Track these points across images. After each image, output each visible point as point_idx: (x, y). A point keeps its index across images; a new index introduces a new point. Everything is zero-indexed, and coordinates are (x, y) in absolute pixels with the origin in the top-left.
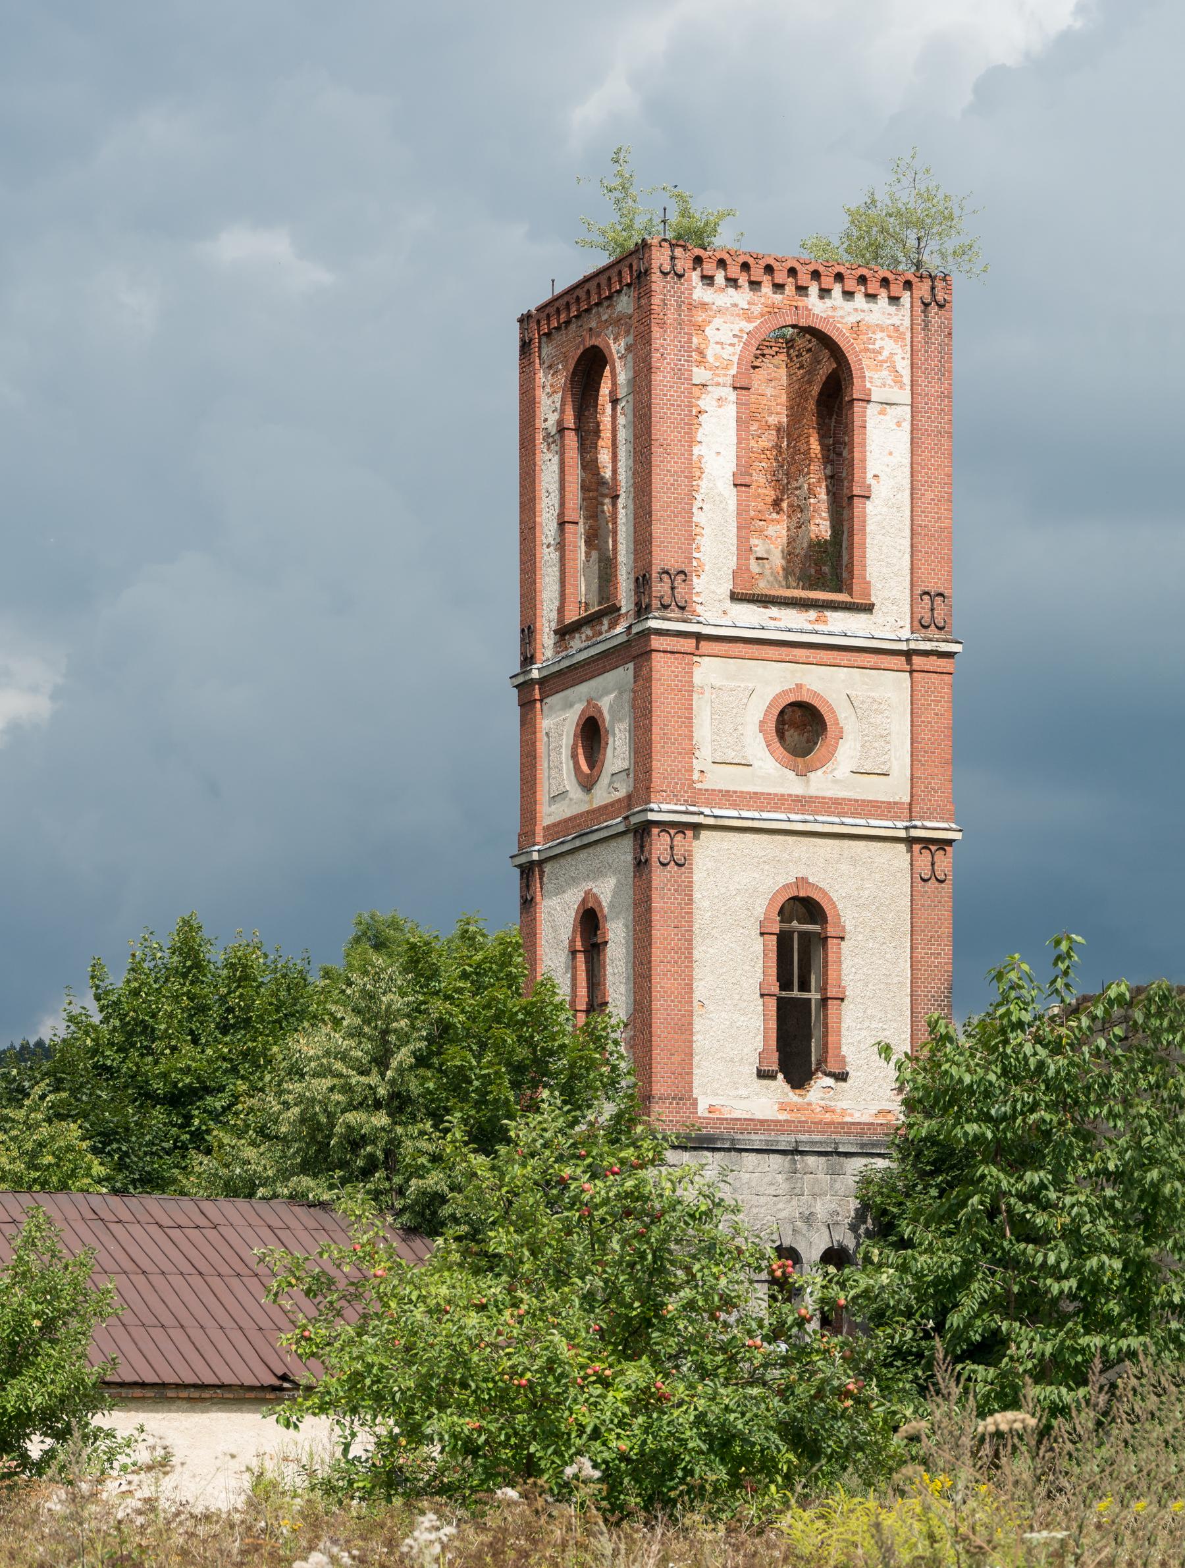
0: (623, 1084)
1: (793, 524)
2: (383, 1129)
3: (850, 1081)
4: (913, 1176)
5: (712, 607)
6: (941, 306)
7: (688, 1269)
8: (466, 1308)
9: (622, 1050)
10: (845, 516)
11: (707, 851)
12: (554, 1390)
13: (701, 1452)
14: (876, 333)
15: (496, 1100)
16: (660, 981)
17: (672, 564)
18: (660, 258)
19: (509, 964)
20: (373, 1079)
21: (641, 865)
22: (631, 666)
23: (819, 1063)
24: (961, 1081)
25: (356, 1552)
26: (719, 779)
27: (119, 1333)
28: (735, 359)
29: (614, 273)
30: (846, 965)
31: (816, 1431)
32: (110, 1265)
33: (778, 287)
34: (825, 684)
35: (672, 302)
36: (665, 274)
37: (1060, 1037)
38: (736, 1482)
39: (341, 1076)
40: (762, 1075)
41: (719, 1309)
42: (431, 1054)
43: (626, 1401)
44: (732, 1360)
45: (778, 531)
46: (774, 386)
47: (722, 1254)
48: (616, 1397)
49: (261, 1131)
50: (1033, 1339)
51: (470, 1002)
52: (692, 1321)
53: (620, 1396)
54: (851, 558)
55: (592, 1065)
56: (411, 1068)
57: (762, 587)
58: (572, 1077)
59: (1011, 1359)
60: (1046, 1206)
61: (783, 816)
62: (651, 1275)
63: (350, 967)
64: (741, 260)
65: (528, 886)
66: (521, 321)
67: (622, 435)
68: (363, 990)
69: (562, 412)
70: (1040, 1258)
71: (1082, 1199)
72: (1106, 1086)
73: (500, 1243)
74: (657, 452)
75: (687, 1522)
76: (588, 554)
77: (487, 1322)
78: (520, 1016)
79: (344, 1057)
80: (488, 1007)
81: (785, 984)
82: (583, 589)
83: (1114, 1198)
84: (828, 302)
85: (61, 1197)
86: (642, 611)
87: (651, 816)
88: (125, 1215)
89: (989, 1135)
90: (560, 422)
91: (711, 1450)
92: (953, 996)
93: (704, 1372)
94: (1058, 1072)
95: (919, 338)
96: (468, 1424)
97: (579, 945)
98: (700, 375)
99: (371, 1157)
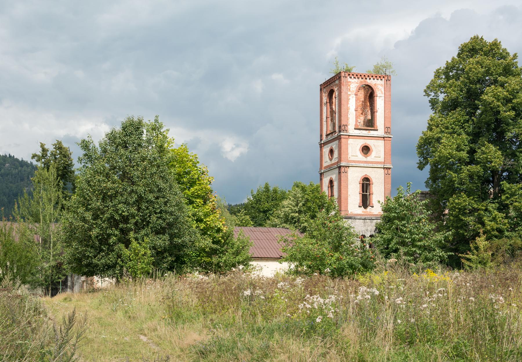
4: (384, 223)
5: (351, 131)
11: (350, 170)
14: (378, 85)
16: (343, 191)
17: (345, 124)
18: (343, 74)
19: (317, 189)
20: (296, 208)
21: (340, 173)
26: (352, 159)
27: (255, 249)
32: (253, 238)
34: (370, 143)
38: (353, 273)
40: (359, 207)
45: (362, 118)
46: (362, 95)
48: (334, 259)
49: (278, 217)
51: (312, 195)
55: (331, 205)
57: (360, 127)
60: (405, 227)
67: (337, 103)
72: (416, 207)
74: (342, 105)
81: (363, 192)
82: (330, 128)
85: (246, 228)
86: (340, 131)
88: (270, 231)
92: (391, 193)
93: (348, 255)
96: (309, 263)
98: (349, 93)
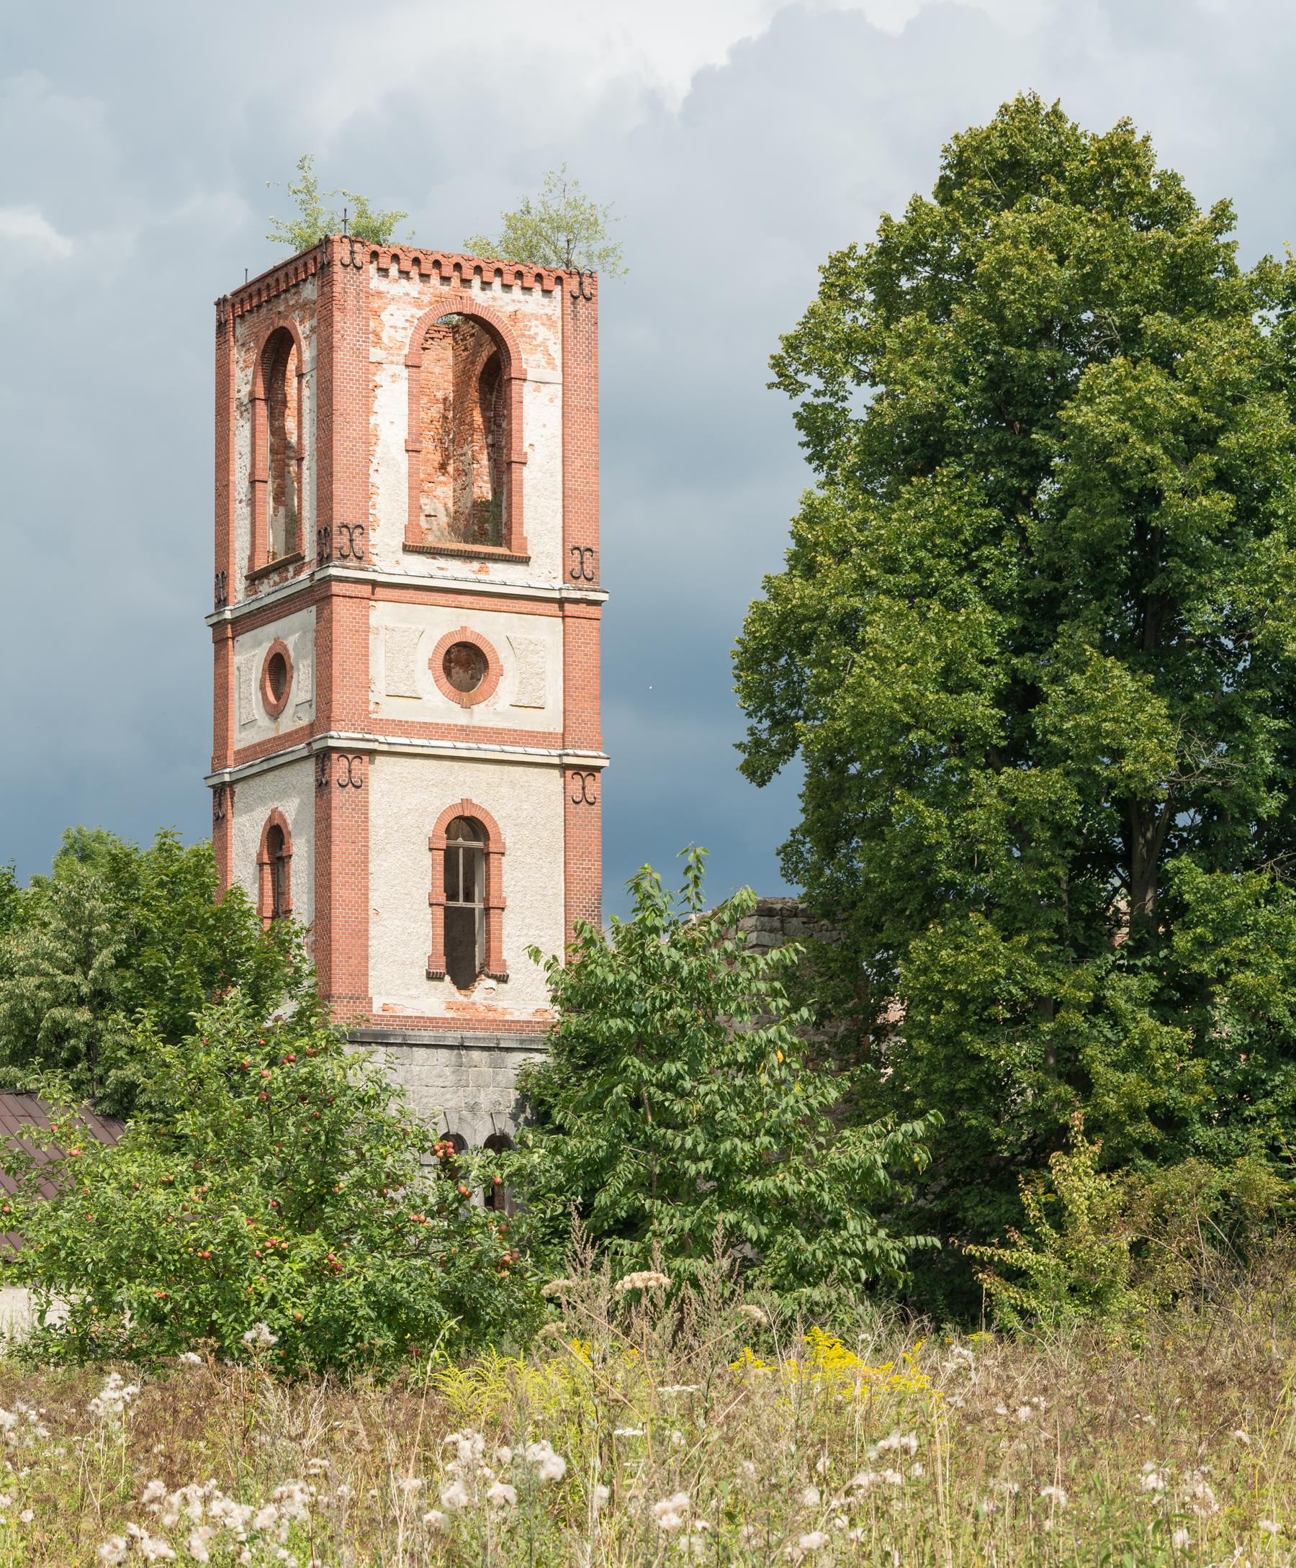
0: (306, 983)
1: (458, 486)
2: (85, 1024)
3: (510, 983)
6: (588, 299)
7: (358, 1150)
8: (155, 1185)
9: (304, 953)
10: (505, 478)
11: (381, 774)
12: (234, 1261)
13: (371, 1320)
14: (531, 321)
15: (189, 998)
17: (351, 519)
18: (341, 252)
20: (77, 978)
21: (322, 786)
22: (314, 608)
23: (482, 966)
24: (605, 980)
25: (43, 1411)
26: (392, 710)
28: (407, 341)
29: (300, 263)
30: (506, 878)
31: (475, 1300)
33: (446, 280)
34: (488, 627)
35: (352, 290)
36: (345, 266)
37: (694, 940)
38: (402, 1348)
39: (47, 974)
40: (431, 977)
41: (386, 1186)
42: (130, 955)
43: (302, 1272)
44: (399, 1233)
46: (442, 366)
47: (389, 1136)
48: (291, 1271)
50: (673, 1216)
52: (362, 1198)
53: (296, 1267)
54: (510, 516)
56: (112, 968)
57: (431, 541)
58: (259, 977)
59: (654, 1233)
60: (682, 1094)
61: (449, 744)
62: (324, 1155)
63: (59, 877)
64: (413, 255)
65: (220, 805)
66: (218, 304)
67: (307, 405)
68: (68, 897)
69: (254, 384)
70: (678, 1142)
71: (715, 1088)
73: (187, 1125)
74: (338, 420)
75: (357, 1384)
76: (275, 510)
77: (173, 1199)
78: (211, 922)
79: (50, 957)
80: (182, 913)
81: (452, 895)
82: (272, 542)
83: (743, 1087)
84: (489, 293)
86: (324, 559)
87: (331, 743)
89: (632, 1029)
90: (252, 393)
91: (379, 1316)
93: (373, 1245)
94: (691, 973)
95: (569, 326)
96: (155, 1293)
97: (266, 859)
99: (74, 1050)
